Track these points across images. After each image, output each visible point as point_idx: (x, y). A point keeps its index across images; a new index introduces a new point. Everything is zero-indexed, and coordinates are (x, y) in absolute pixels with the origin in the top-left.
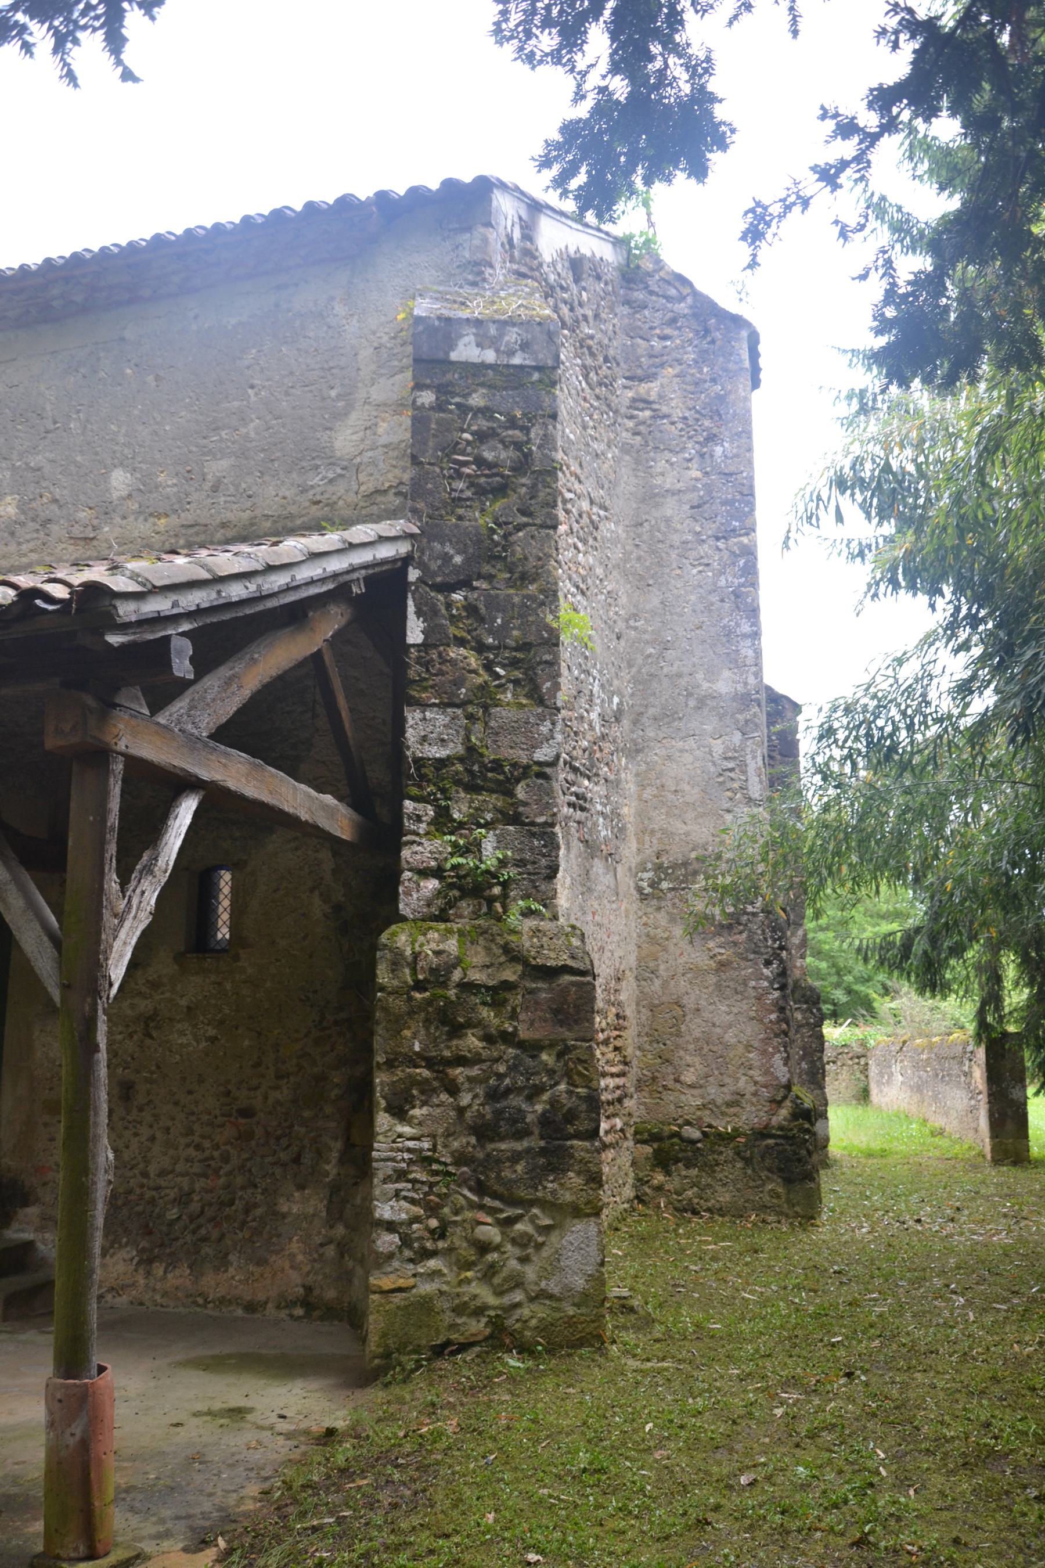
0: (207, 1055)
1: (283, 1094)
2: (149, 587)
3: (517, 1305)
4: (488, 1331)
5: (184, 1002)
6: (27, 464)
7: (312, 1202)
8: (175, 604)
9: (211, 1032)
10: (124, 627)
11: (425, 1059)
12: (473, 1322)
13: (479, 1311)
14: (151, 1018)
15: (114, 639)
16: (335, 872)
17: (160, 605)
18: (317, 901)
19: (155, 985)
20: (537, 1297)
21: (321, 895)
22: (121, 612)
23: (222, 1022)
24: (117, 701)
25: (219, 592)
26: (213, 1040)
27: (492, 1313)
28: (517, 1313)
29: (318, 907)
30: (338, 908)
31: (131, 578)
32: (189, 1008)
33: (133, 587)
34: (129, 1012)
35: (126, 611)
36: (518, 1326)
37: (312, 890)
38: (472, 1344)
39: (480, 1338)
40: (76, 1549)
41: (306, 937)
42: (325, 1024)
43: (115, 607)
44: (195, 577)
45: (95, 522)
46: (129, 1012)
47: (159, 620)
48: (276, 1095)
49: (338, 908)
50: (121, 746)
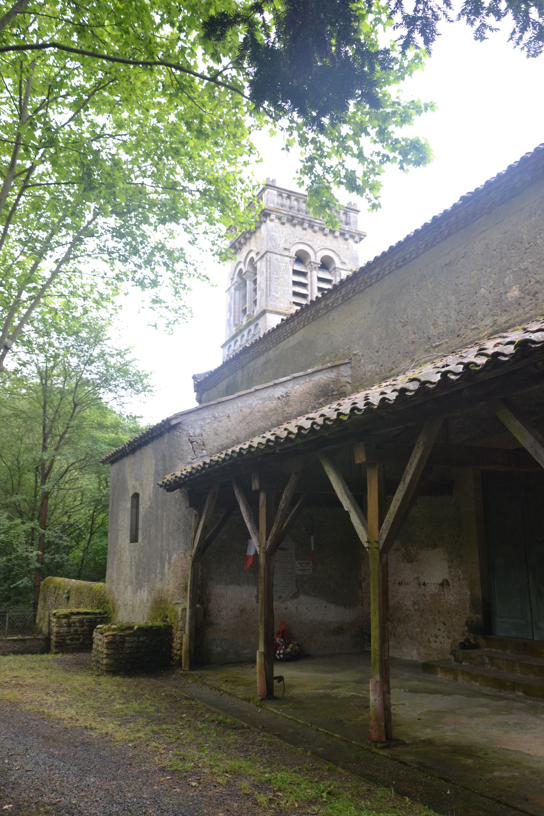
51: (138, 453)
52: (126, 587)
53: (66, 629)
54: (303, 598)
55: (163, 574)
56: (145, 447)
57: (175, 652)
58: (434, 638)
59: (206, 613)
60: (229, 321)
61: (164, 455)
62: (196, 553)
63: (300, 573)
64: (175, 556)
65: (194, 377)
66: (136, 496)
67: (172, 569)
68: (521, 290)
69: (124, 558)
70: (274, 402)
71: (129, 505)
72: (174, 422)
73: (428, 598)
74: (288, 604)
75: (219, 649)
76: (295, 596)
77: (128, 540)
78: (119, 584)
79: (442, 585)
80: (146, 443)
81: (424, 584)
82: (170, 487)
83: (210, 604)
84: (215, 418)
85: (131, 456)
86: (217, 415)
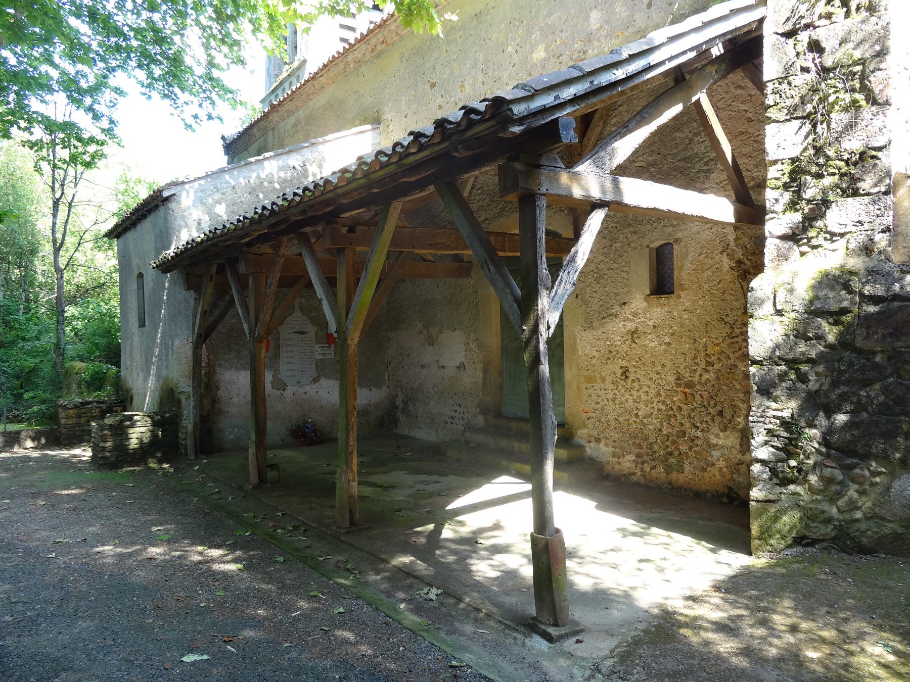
0: (666, 352)
1: (711, 376)
2: (532, 91)
3: (857, 520)
4: (833, 534)
5: (651, 323)
6: (547, 24)
7: (731, 439)
8: (557, 98)
9: (667, 340)
10: (521, 120)
11: (783, 360)
12: (822, 527)
13: (828, 521)
14: (635, 332)
15: (516, 129)
16: (736, 240)
17: (547, 100)
18: (725, 259)
19: (635, 314)
20: (872, 518)
21: (728, 255)
22: (515, 112)
23: (673, 334)
24: (541, 163)
25: (592, 82)
26: (669, 344)
27: (837, 523)
28: (857, 526)
29: (726, 263)
30: (739, 262)
31: (522, 89)
32: (654, 327)
33: (521, 94)
34: (623, 330)
35: (519, 110)
36: (857, 534)
37: (721, 253)
38: (823, 541)
39: (828, 537)
40: (548, 620)
41: (719, 283)
42: (734, 334)
43: (511, 110)
44: (568, 77)
45: (585, 49)
46: (623, 330)
47: (545, 110)
48: (706, 376)
49: (739, 262)
50: (543, 190)
51: (139, 227)
52: (138, 374)
53: (75, 420)
54: (324, 382)
55: (168, 362)
56: (144, 221)
57: (181, 441)
58: (451, 420)
59: (214, 401)
60: (268, 69)
61: (161, 231)
62: (197, 340)
63: (320, 357)
64: (177, 342)
65: (223, 138)
66: (141, 275)
67: (174, 356)
68: (546, 50)
69: (135, 344)
70: (289, 172)
71: (135, 287)
72: (166, 194)
73: (446, 380)
74: (308, 388)
75: (232, 436)
76: (316, 380)
77: (137, 325)
78: (132, 371)
79: (458, 368)
80: (144, 216)
81: (443, 367)
82: (165, 267)
83: (219, 392)
84: (218, 190)
85: (133, 230)
86: (219, 186)
